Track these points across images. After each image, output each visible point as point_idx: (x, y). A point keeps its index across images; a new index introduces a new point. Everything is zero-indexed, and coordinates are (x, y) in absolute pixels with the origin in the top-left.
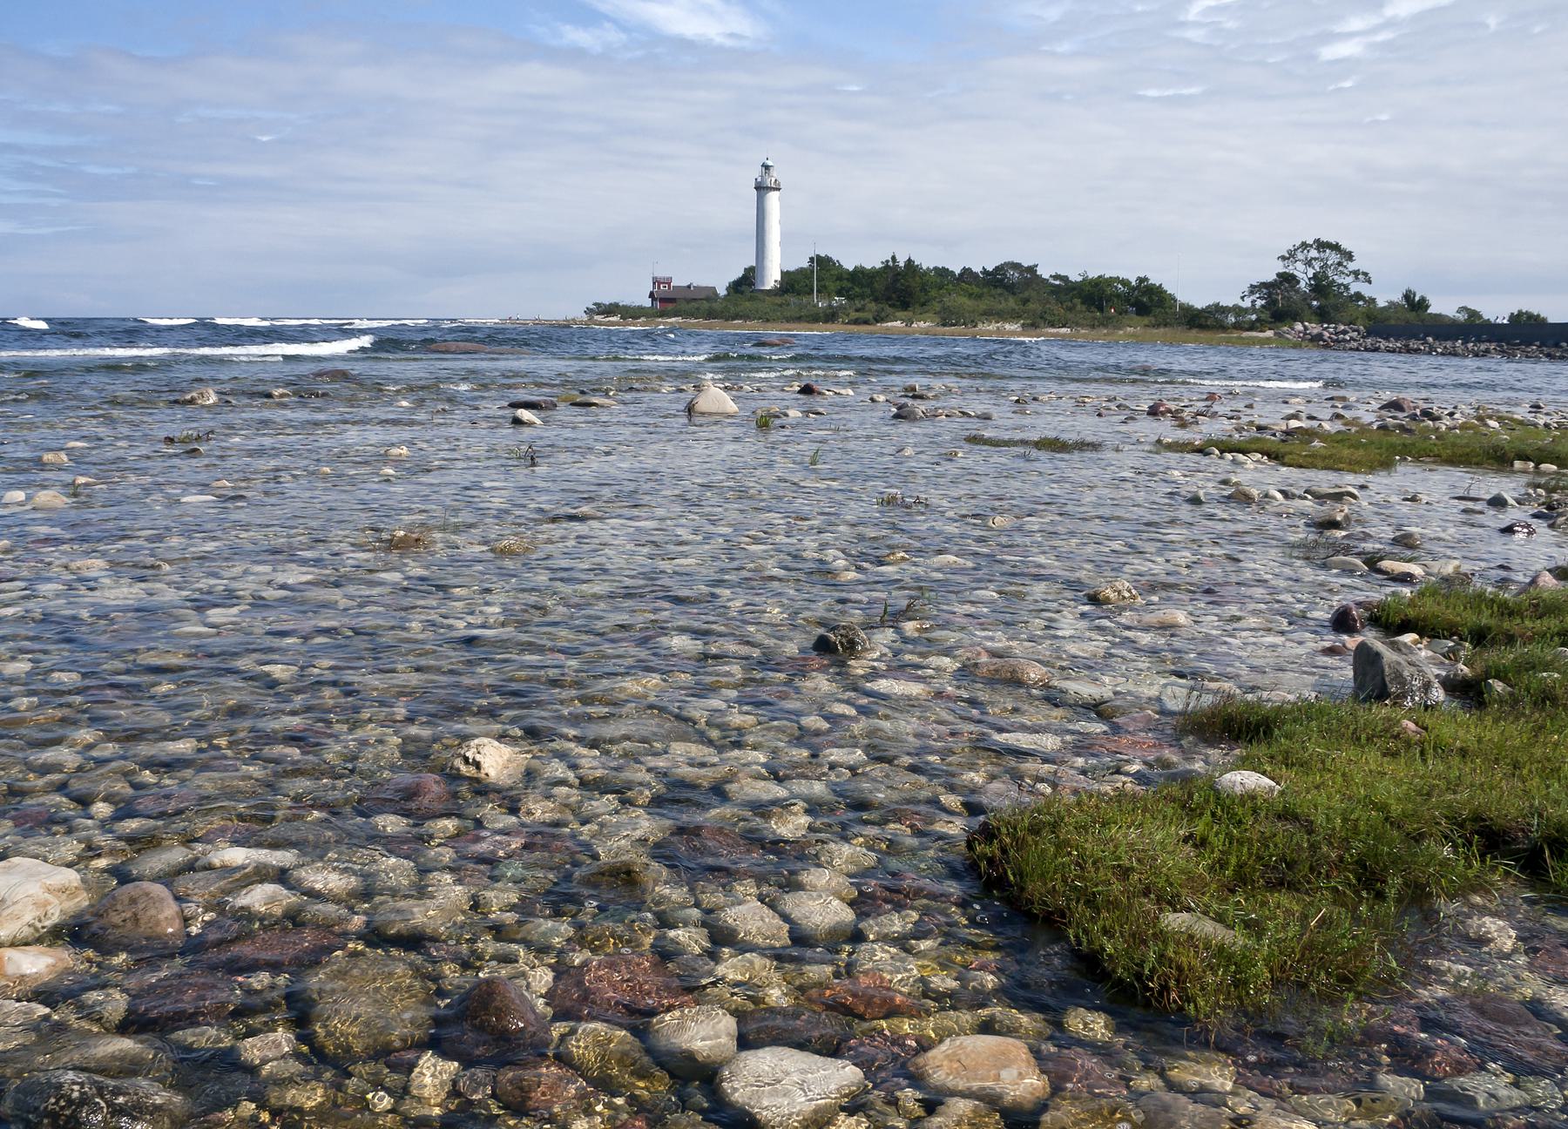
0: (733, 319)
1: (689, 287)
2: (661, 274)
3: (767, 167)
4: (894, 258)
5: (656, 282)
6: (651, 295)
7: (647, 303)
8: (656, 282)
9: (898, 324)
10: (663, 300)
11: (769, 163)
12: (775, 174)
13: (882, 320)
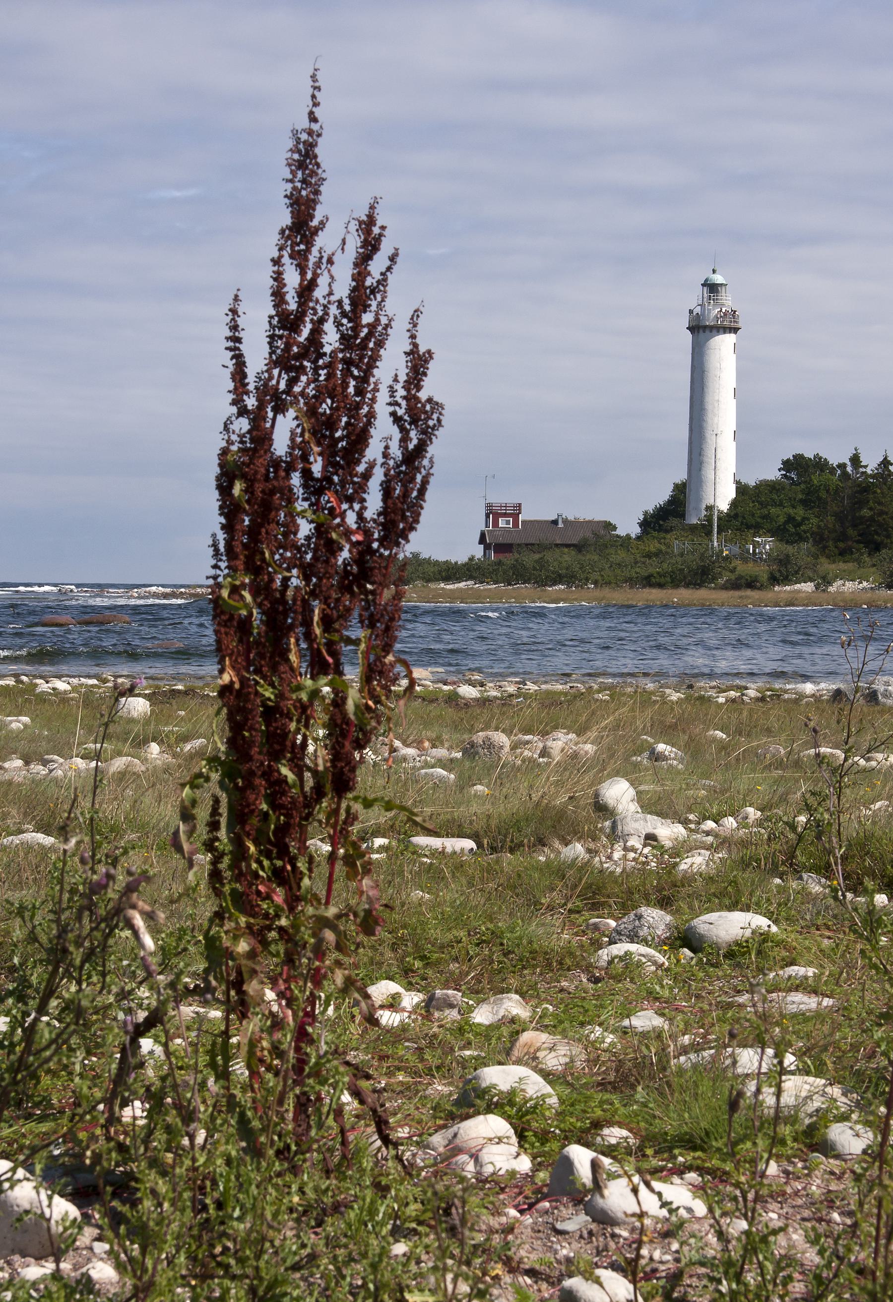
0: (555, 583)
1: (555, 522)
2: (502, 498)
3: (712, 288)
4: (855, 460)
5: (493, 513)
6: (482, 540)
7: (478, 552)
8: (493, 513)
9: (808, 587)
10: (502, 548)
11: (718, 279)
12: (728, 301)
13: (786, 579)
